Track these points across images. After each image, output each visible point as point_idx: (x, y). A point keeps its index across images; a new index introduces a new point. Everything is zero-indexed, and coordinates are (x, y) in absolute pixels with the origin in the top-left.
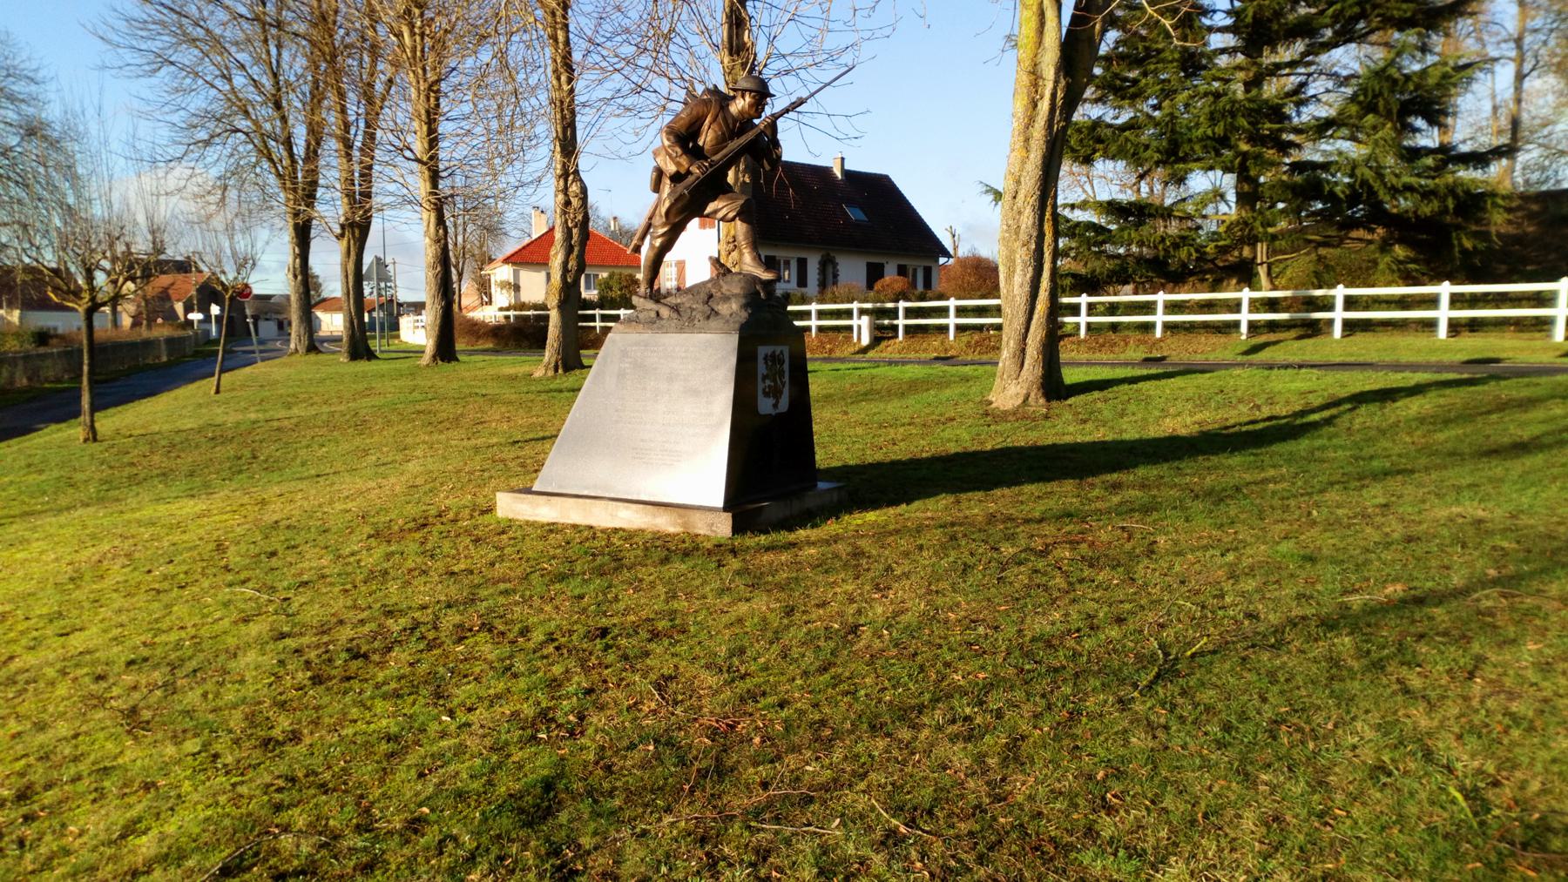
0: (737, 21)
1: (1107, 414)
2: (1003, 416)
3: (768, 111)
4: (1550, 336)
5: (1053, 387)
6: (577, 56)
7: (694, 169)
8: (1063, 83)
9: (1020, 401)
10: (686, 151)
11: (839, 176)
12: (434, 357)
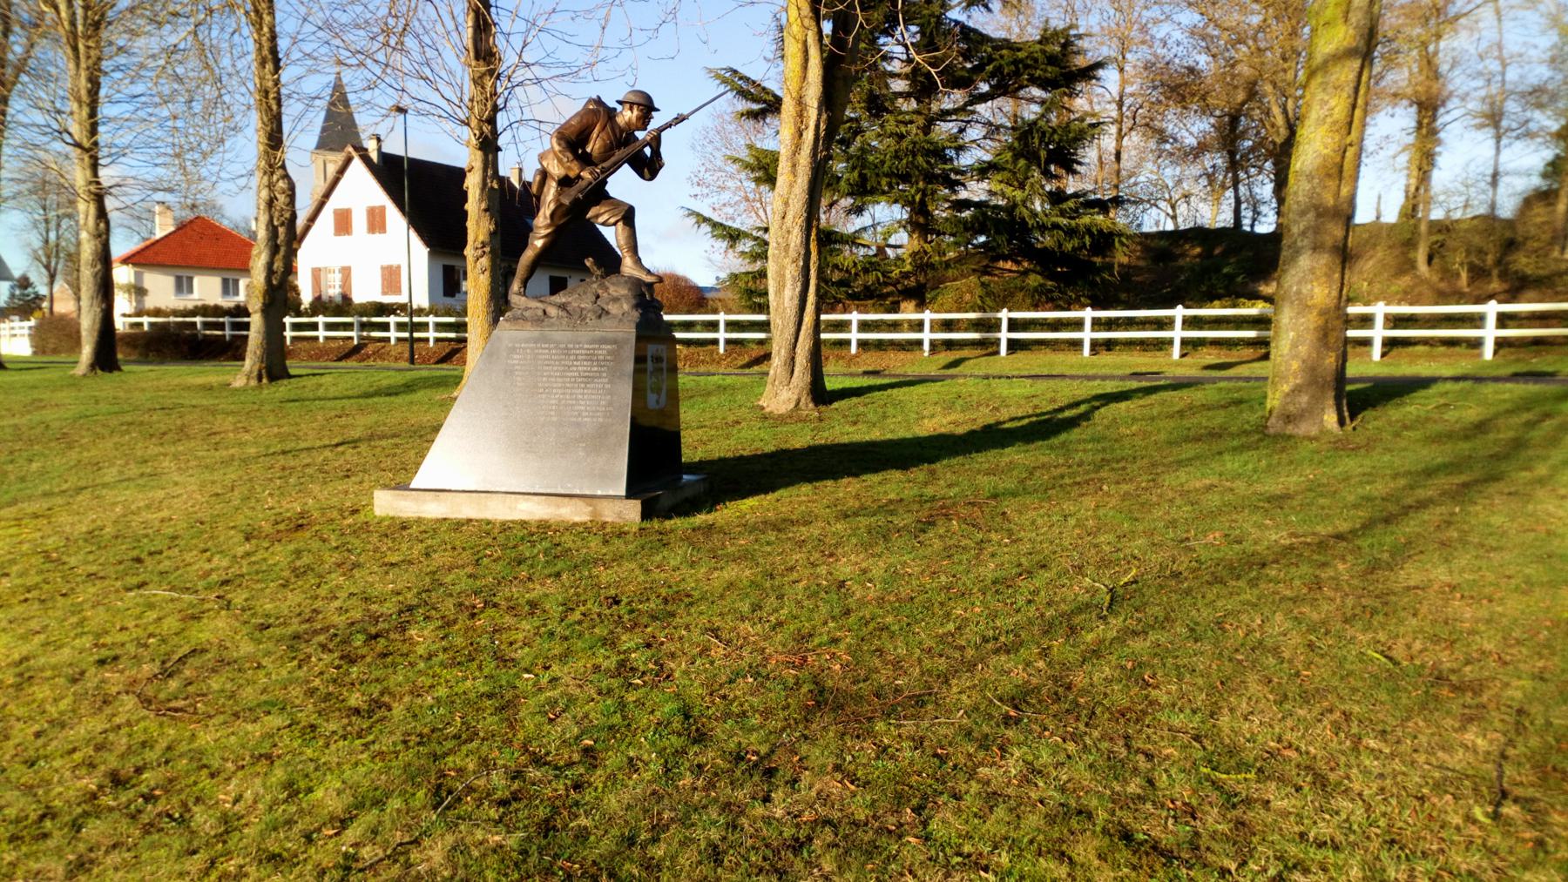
0: (483, 27)
1: (871, 417)
2: (782, 420)
3: (654, 124)
4: (1170, 355)
5: (820, 394)
6: (283, 44)
7: (586, 174)
8: (824, 116)
9: (792, 406)
10: (577, 157)
11: (517, 185)
12: (93, 366)
